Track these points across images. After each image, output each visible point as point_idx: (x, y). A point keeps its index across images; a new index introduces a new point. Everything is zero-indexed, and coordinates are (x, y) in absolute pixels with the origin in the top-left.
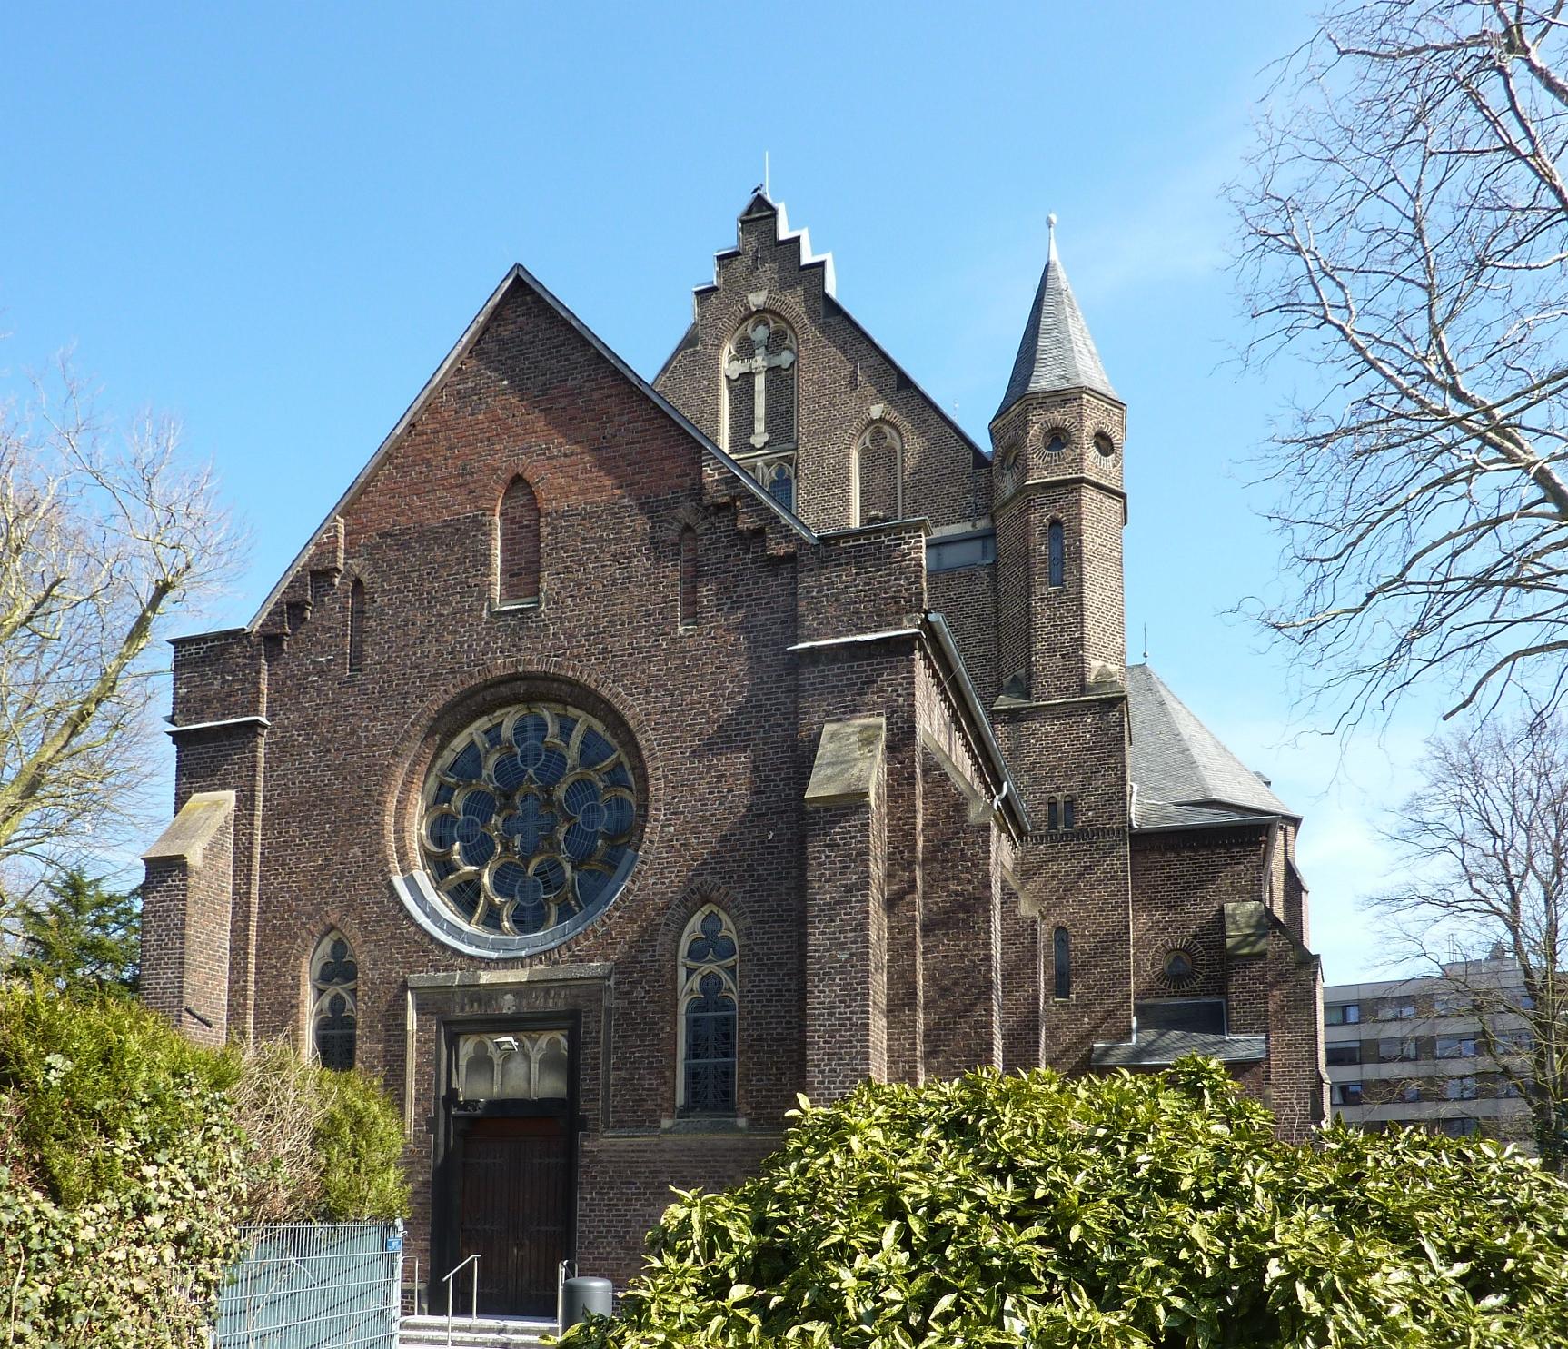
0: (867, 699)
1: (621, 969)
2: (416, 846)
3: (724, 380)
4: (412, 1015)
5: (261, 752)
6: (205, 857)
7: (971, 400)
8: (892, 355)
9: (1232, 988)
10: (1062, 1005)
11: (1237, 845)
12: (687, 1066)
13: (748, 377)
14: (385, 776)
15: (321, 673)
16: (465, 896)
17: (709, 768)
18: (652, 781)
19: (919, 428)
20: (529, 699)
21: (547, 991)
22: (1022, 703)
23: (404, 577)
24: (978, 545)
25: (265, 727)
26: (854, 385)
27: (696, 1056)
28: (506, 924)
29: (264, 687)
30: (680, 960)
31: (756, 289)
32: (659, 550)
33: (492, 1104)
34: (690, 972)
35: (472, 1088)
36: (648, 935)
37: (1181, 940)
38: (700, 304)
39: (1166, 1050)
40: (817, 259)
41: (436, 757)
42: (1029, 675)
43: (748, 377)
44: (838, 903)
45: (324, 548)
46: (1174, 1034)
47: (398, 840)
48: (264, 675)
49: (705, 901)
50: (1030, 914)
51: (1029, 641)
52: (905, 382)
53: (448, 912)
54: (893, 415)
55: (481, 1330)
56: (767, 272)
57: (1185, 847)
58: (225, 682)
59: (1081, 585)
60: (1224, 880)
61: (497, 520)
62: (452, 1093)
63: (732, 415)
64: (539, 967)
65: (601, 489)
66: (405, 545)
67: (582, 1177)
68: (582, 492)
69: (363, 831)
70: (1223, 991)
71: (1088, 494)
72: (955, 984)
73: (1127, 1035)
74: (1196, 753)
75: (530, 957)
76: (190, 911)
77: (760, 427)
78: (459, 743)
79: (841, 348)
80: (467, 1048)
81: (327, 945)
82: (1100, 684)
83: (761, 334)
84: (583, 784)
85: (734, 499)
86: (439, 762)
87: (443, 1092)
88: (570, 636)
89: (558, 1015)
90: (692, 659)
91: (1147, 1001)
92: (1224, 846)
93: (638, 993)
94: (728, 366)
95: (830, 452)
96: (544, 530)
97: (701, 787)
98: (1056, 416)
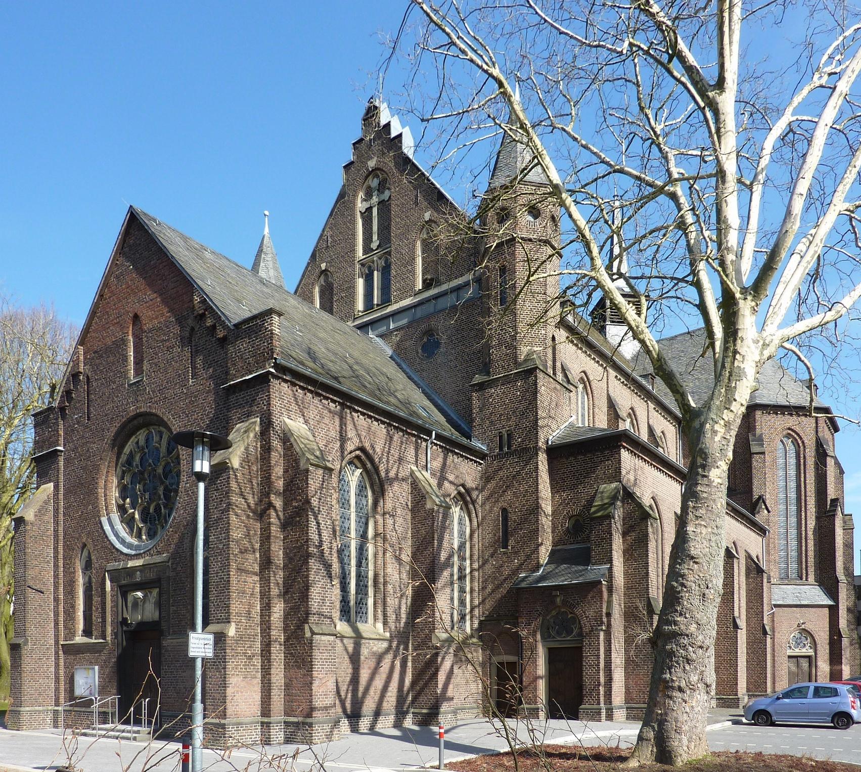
3: (359, 214)
4: (108, 583)
5: (61, 463)
6: (36, 516)
10: (505, 553)
13: (369, 209)
14: (97, 468)
15: (78, 423)
16: (129, 522)
20: (146, 425)
21: (150, 569)
25: (62, 451)
26: (416, 203)
28: (144, 537)
29: (61, 433)
35: (135, 618)
38: (346, 173)
41: (118, 458)
43: (369, 209)
48: (61, 426)
53: (123, 534)
60: (599, 471)
61: (131, 338)
62: (125, 620)
65: (162, 315)
67: (163, 659)
69: (92, 497)
73: (538, 566)
77: (375, 237)
78: (127, 450)
80: (130, 599)
81: (85, 553)
87: (120, 619)
88: (154, 392)
90: (195, 397)
91: (559, 547)
94: (361, 206)
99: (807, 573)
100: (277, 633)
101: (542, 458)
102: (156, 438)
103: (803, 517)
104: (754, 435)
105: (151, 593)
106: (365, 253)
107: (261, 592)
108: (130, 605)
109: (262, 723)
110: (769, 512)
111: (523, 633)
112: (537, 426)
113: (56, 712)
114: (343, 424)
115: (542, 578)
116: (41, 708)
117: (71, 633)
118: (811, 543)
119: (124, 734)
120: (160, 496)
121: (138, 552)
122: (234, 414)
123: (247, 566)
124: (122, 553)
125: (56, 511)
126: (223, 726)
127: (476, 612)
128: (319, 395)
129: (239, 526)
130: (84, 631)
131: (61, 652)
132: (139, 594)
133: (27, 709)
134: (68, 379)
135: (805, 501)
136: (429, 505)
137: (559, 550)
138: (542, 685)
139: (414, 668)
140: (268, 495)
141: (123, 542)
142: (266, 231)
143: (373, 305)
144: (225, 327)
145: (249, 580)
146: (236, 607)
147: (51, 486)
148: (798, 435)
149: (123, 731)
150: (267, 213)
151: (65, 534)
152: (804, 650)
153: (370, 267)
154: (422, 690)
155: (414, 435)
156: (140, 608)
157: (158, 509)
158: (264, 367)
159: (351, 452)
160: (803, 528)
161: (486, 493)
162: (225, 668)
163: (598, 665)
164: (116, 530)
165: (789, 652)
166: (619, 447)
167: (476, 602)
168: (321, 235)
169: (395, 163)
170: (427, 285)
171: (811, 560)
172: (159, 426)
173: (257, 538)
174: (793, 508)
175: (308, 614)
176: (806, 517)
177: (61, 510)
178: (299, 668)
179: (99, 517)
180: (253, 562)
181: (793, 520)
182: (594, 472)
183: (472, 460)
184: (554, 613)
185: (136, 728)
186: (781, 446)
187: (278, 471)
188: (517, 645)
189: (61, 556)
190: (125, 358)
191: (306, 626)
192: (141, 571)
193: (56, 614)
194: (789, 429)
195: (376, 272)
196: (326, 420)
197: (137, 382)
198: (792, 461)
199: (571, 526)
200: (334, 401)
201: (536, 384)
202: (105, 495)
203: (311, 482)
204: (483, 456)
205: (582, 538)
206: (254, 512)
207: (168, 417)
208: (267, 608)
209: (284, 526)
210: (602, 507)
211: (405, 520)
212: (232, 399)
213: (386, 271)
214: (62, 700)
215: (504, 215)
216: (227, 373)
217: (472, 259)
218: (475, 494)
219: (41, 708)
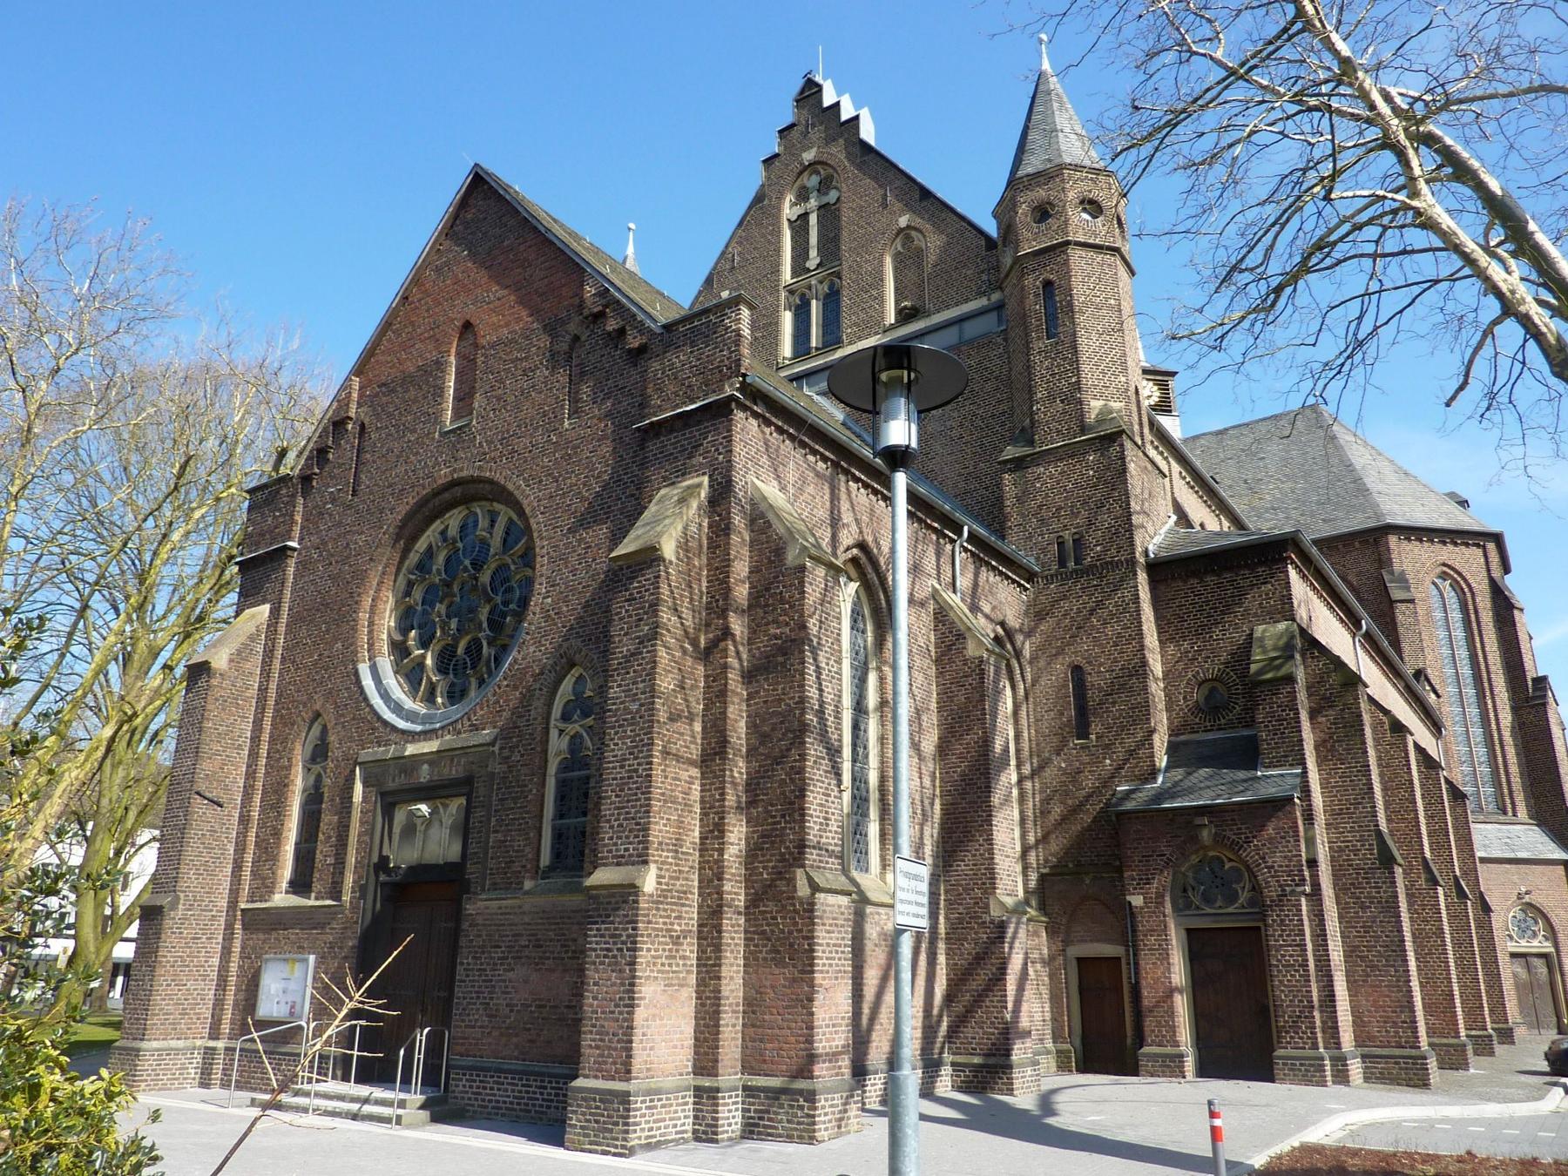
0: (694, 461)
1: (505, 735)
2: (385, 637)
3: (786, 224)
4: (358, 788)
5: (291, 570)
6: (231, 661)
7: (976, 196)
8: (913, 175)
9: (1260, 718)
11: (1261, 563)
12: (554, 828)
13: (804, 217)
14: (360, 576)
15: (333, 501)
16: (412, 675)
17: (580, 541)
18: (539, 559)
19: (938, 228)
20: (466, 500)
22: (1027, 450)
23: (390, 415)
24: (993, 316)
25: (294, 549)
27: (562, 816)
28: (439, 700)
29: (298, 518)
30: (553, 722)
31: (808, 148)
32: (554, 360)
33: (411, 869)
34: (561, 731)
35: (403, 856)
36: (526, 700)
37: (1212, 669)
39: (1190, 791)
40: (854, 114)
42: (1033, 422)
43: (804, 217)
44: (633, 655)
45: (342, 401)
46: (1204, 772)
47: (370, 632)
48: (300, 508)
49: (572, 665)
50: (977, 654)
51: (1031, 392)
52: (926, 194)
53: (398, 692)
54: (918, 222)
55: (341, 1098)
56: (816, 134)
57: (1206, 573)
58: (275, 517)
59: (1074, 334)
60: (1252, 601)
61: (453, 359)
62: (384, 860)
63: (793, 248)
64: (448, 737)
65: (519, 319)
66: (393, 391)
67: (463, 942)
68: (507, 325)
69: (345, 627)
70: (1251, 723)
71: (1077, 257)
72: (773, 729)
73: (1153, 773)
74: (1371, 481)
75: (442, 728)
76: (209, 707)
77: (813, 253)
78: (421, 545)
79: (875, 179)
80: (400, 816)
81: (316, 730)
82: (1100, 421)
83: (813, 181)
84: (502, 568)
85: (606, 306)
86: (407, 563)
87: (375, 859)
88: (489, 443)
89: (453, 782)
91: (1182, 738)
92: (1247, 566)
93: (516, 757)
94: (789, 211)
95: (867, 261)
96: (480, 360)
97: (573, 559)
98: (1041, 193)
99: (1513, 803)
100: (735, 891)
101: (1142, 577)
102: (483, 523)
103: (1490, 706)
104: (1392, 573)
105: (445, 806)
106: (795, 274)
107: (702, 801)
108: (397, 830)
109: (697, 1089)
110: (1438, 696)
111: (1137, 900)
112: (1131, 525)
113: (209, 1053)
114: (834, 498)
115: (1160, 796)
116: (181, 1044)
117: (264, 886)
118: (1511, 752)
119: (367, 1109)
120: (480, 624)
121: (428, 727)
122: (654, 475)
123: (678, 746)
124: (394, 729)
125: (269, 653)
126: (624, 1098)
127: (1032, 858)
128: (803, 445)
129: (673, 672)
130: (292, 883)
131: (238, 926)
132: (424, 808)
133: (155, 1044)
134: (325, 429)
135: (1489, 680)
136: (971, 650)
137: (1185, 743)
138: (1181, 1004)
139: (951, 967)
140: (723, 614)
141: (398, 709)
142: (630, 250)
143: (810, 348)
144: (641, 328)
145: (684, 775)
146: (660, 829)
147: (265, 609)
148: (1460, 574)
149: (366, 1101)
150: (632, 226)
151: (280, 695)
152: (1535, 943)
153: (803, 296)
154: (969, 1012)
155: (935, 530)
156: (419, 836)
157: (474, 649)
158: (722, 390)
159: (848, 549)
160: (1494, 726)
161: (1037, 639)
162: (633, 963)
163: (1305, 965)
164: (384, 686)
165: (1512, 947)
166: (1284, 561)
167: (1031, 839)
168: (723, 253)
169: (848, 153)
170: (905, 316)
171: (1516, 780)
172: (492, 500)
173: (699, 693)
174: (1470, 692)
175: (802, 846)
176: (1495, 706)
177: (279, 653)
178: (780, 963)
179: (355, 663)
180: (689, 738)
181: (1473, 712)
182: (1240, 604)
183: (1014, 581)
184: (1194, 859)
185: (402, 1096)
186: (1435, 592)
187: (741, 568)
188: (1126, 926)
189: (266, 737)
190: (439, 391)
191: (799, 873)
192: (431, 763)
193: (240, 848)
194: (1444, 565)
195: (814, 302)
196: (811, 489)
197: (459, 428)
198: (1456, 615)
199: (1202, 701)
200: (825, 459)
201: (1123, 458)
202: (371, 623)
203: (808, 589)
204: (1031, 576)
205: (1238, 714)
206: (695, 643)
207: (515, 484)
208: (714, 832)
209: (749, 676)
210: (1270, 664)
211: (926, 677)
212: (653, 446)
213: (832, 301)
214: (226, 1028)
215: (1043, 213)
216: (642, 406)
217: (984, 277)
218: (1019, 638)
219: (181, 1044)
